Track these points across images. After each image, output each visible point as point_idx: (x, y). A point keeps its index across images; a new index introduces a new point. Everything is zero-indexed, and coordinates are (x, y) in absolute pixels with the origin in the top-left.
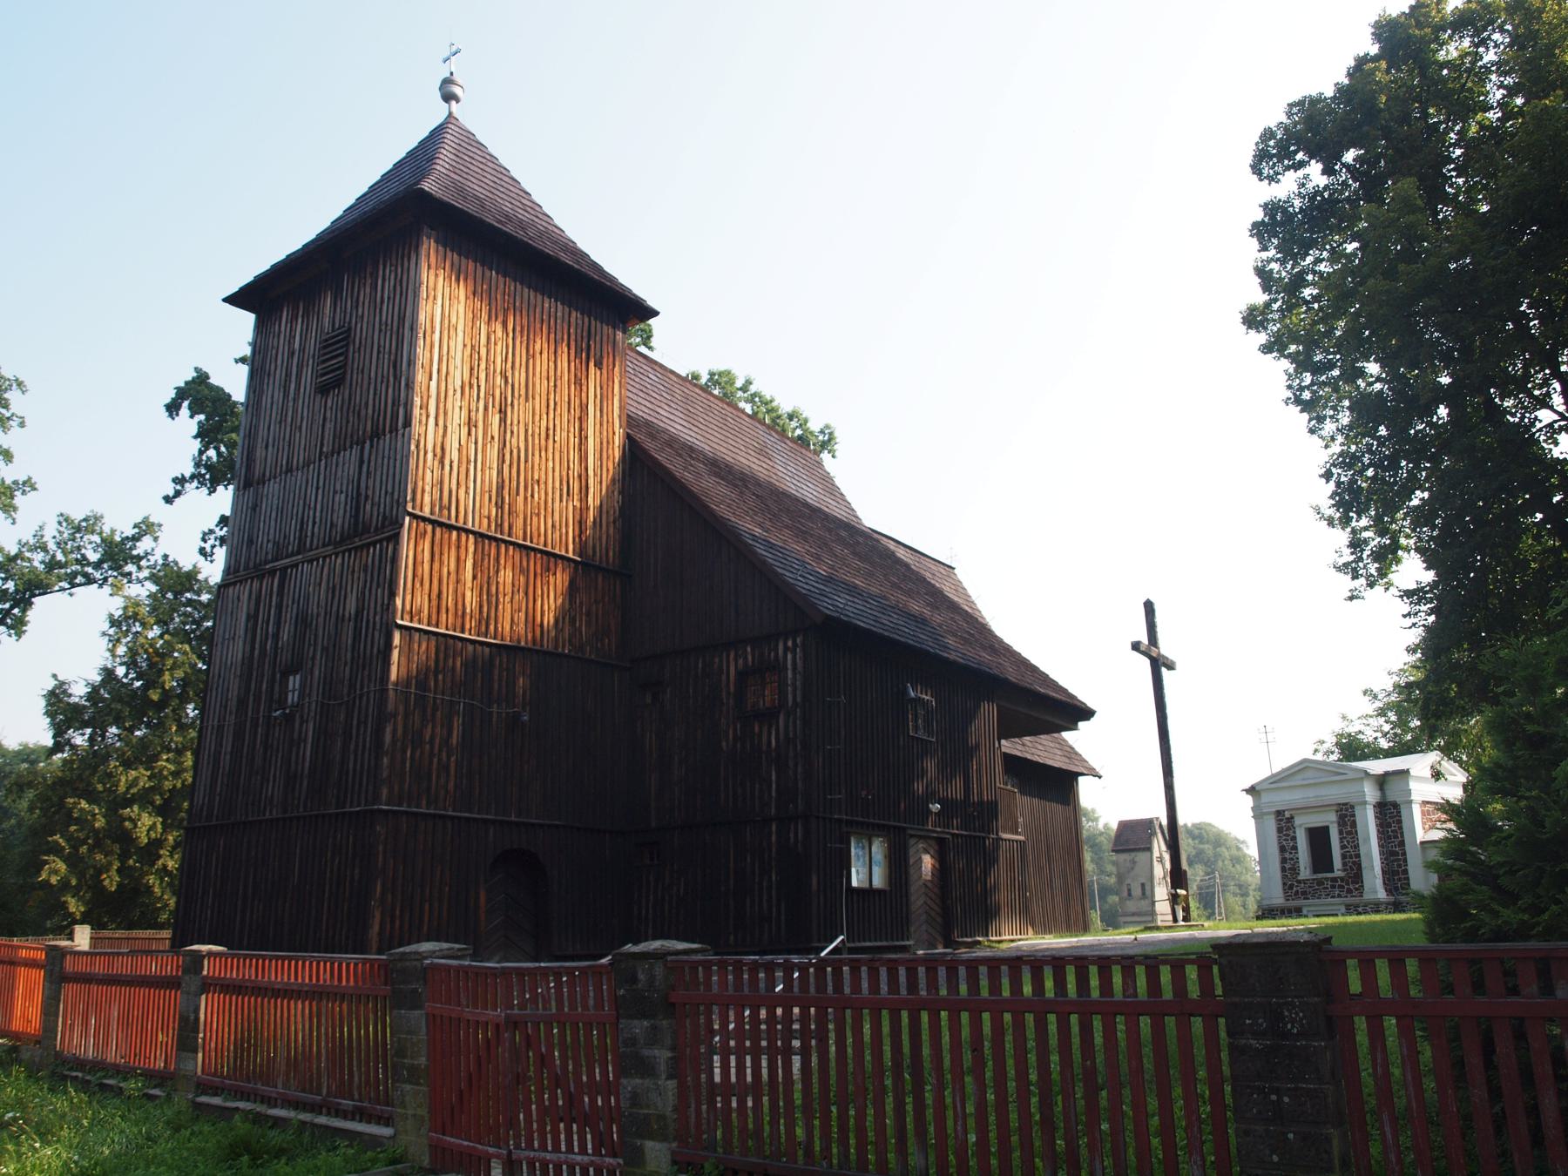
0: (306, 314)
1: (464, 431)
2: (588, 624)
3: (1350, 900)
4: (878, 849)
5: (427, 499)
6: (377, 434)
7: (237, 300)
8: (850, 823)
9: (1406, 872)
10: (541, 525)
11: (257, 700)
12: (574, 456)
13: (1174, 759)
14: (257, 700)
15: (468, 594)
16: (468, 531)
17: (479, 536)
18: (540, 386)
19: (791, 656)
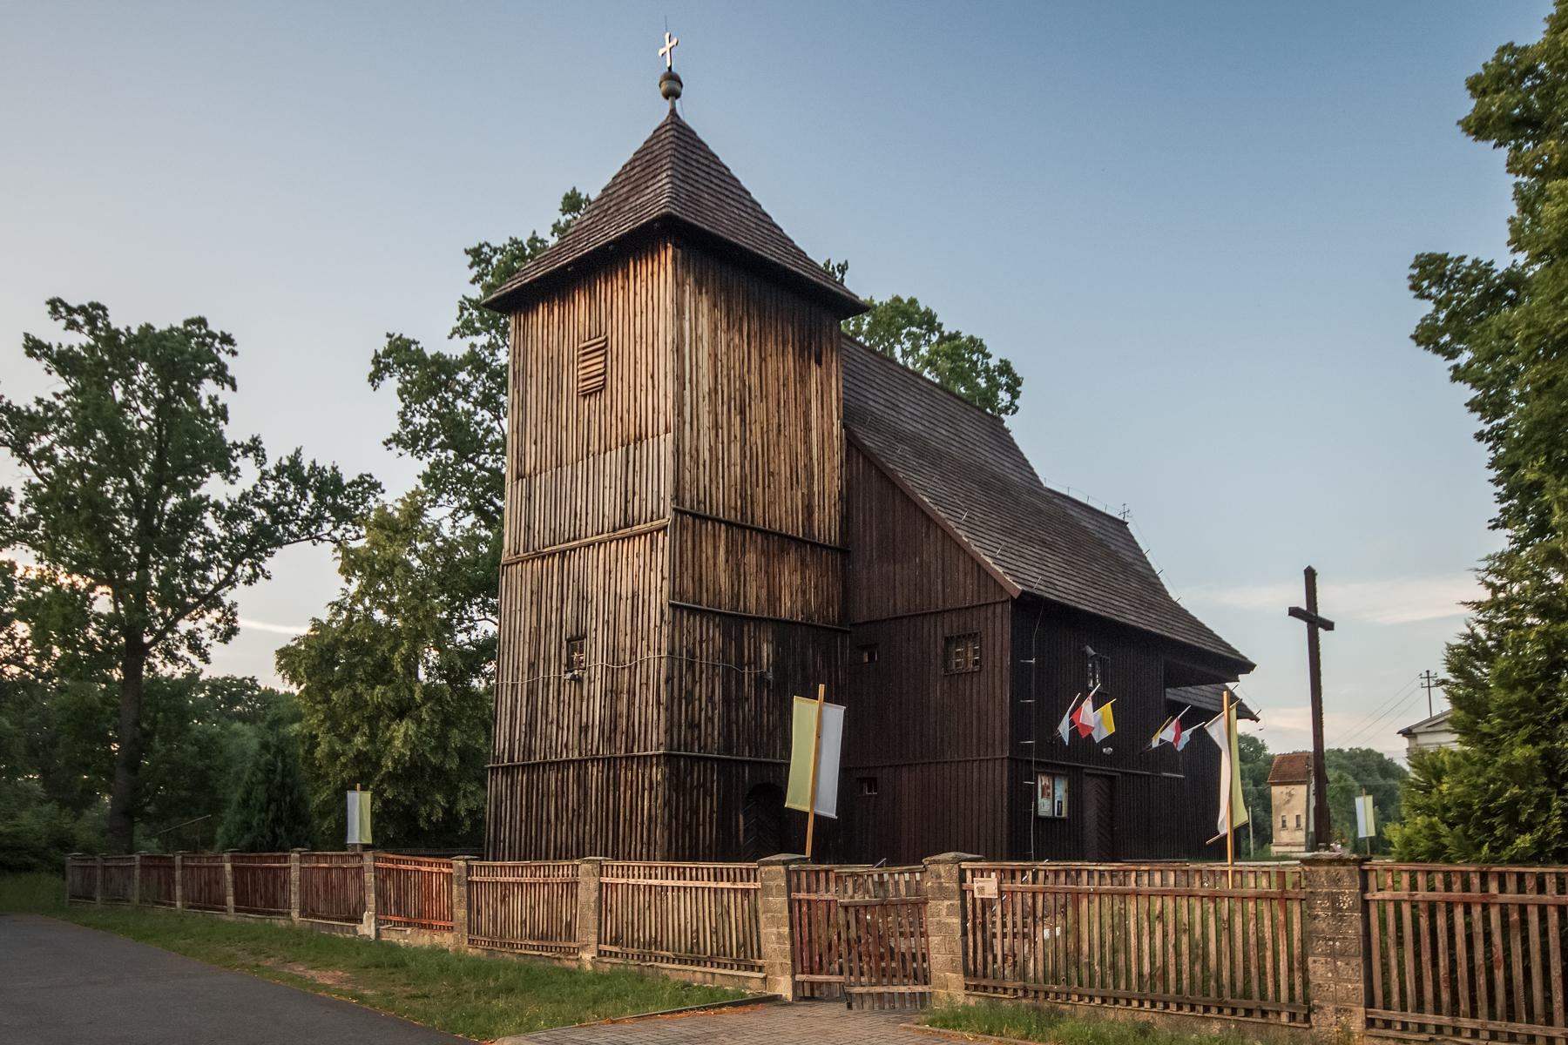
1: (713, 433)
2: (816, 594)
5: (687, 496)
6: (639, 439)
7: (467, 252)
10: (780, 511)
11: (547, 661)
12: (801, 448)
13: (1322, 658)
15: (722, 575)
16: (720, 521)
17: (729, 524)
19: (1000, 629)
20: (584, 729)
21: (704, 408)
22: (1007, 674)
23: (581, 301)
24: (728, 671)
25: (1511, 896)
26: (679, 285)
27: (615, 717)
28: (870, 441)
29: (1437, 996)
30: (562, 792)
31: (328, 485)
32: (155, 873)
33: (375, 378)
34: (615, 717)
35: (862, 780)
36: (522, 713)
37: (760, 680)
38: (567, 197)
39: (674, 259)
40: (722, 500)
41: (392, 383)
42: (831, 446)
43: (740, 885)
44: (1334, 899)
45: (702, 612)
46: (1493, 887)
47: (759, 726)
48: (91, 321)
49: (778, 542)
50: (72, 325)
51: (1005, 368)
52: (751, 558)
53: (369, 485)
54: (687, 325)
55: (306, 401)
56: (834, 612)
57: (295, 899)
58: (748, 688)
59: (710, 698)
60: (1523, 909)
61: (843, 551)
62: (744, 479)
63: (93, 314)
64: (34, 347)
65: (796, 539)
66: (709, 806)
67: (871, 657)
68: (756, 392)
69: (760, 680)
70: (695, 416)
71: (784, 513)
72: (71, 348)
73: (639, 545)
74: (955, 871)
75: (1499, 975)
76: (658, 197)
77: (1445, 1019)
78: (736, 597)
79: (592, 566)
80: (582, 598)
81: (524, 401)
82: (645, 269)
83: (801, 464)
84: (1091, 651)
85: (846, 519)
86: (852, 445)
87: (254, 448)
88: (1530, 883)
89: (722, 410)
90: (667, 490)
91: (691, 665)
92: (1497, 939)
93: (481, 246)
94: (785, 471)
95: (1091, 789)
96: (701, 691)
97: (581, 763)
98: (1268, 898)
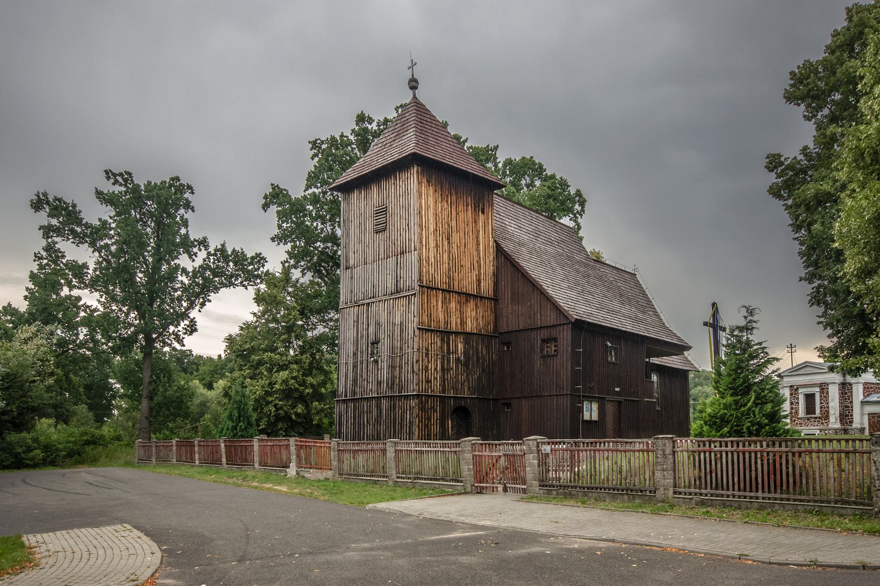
0: (366, 197)
3: (822, 427)
4: (595, 406)
6: (402, 253)
7: (310, 142)
8: (583, 396)
9: (852, 415)
10: (465, 283)
11: (362, 352)
12: (475, 253)
14: (362, 352)
17: (443, 290)
18: (462, 226)
19: (565, 336)
20: (379, 383)
21: (431, 238)
22: (569, 356)
23: (375, 189)
24: (443, 356)
25: (718, 448)
26: (420, 183)
27: (393, 378)
28: (504, 245)
29: (695, 483)
30: (370, 412)
31: (239, 258)
32: (183, 449)
33: (265, 207)
34: (393, 378)
35: (504, 404)
36: (350, 375)
37: (458, 360)
38: (358, 116)
39: (417, 172)
40: (440, 280)
41: (274, 209)
42: (489, 252)
43: (453, 449)
44: (664, 451)
45: (432, 331)
46: (712, 446)
47: (457, 381)
48: (126, 180)
49: (466, 296)
50: (116, 182)
51: (579, 193)
52: (453, 305)
53: (259, 259)
54: (423, 201)
55: (234, 220)
56: (491, 327)
57: (256, 459)
58: (453, 365)
59: (436, 369)
60: (721, 452)
61: (495, 299)
62: (449, 270)
63: (127, 177)
64: (99, 194)
65: (473, 295)
66: (436, 416)
67: (508, 348)
68: (454, 229)
69: (458, 360)
70: (427, 243)
71: (468, 284)
72: (113, 192)
73: (404, 301)
74: (535, 443)
75: (714, 475)
76: (408, 144)
77: (697, 490)
78: (446, 323)
79: (381, 311)
80: (378, 324)
81: (348, 233)
82: (404, 176)
83: (475, 261)
84: (609, 344)
85: (496, 284)
86: (499, 250)
87: (203, 243)
88: (723, 444)
89: (439, 239)
90: (416, 277)
91: (427, 354)
92: (713, 463)
93: (316, 140)
94: (468, 264)
95: (610, 409)
96: (431, 366)
97: (378, 399)
98: (643, 451)
